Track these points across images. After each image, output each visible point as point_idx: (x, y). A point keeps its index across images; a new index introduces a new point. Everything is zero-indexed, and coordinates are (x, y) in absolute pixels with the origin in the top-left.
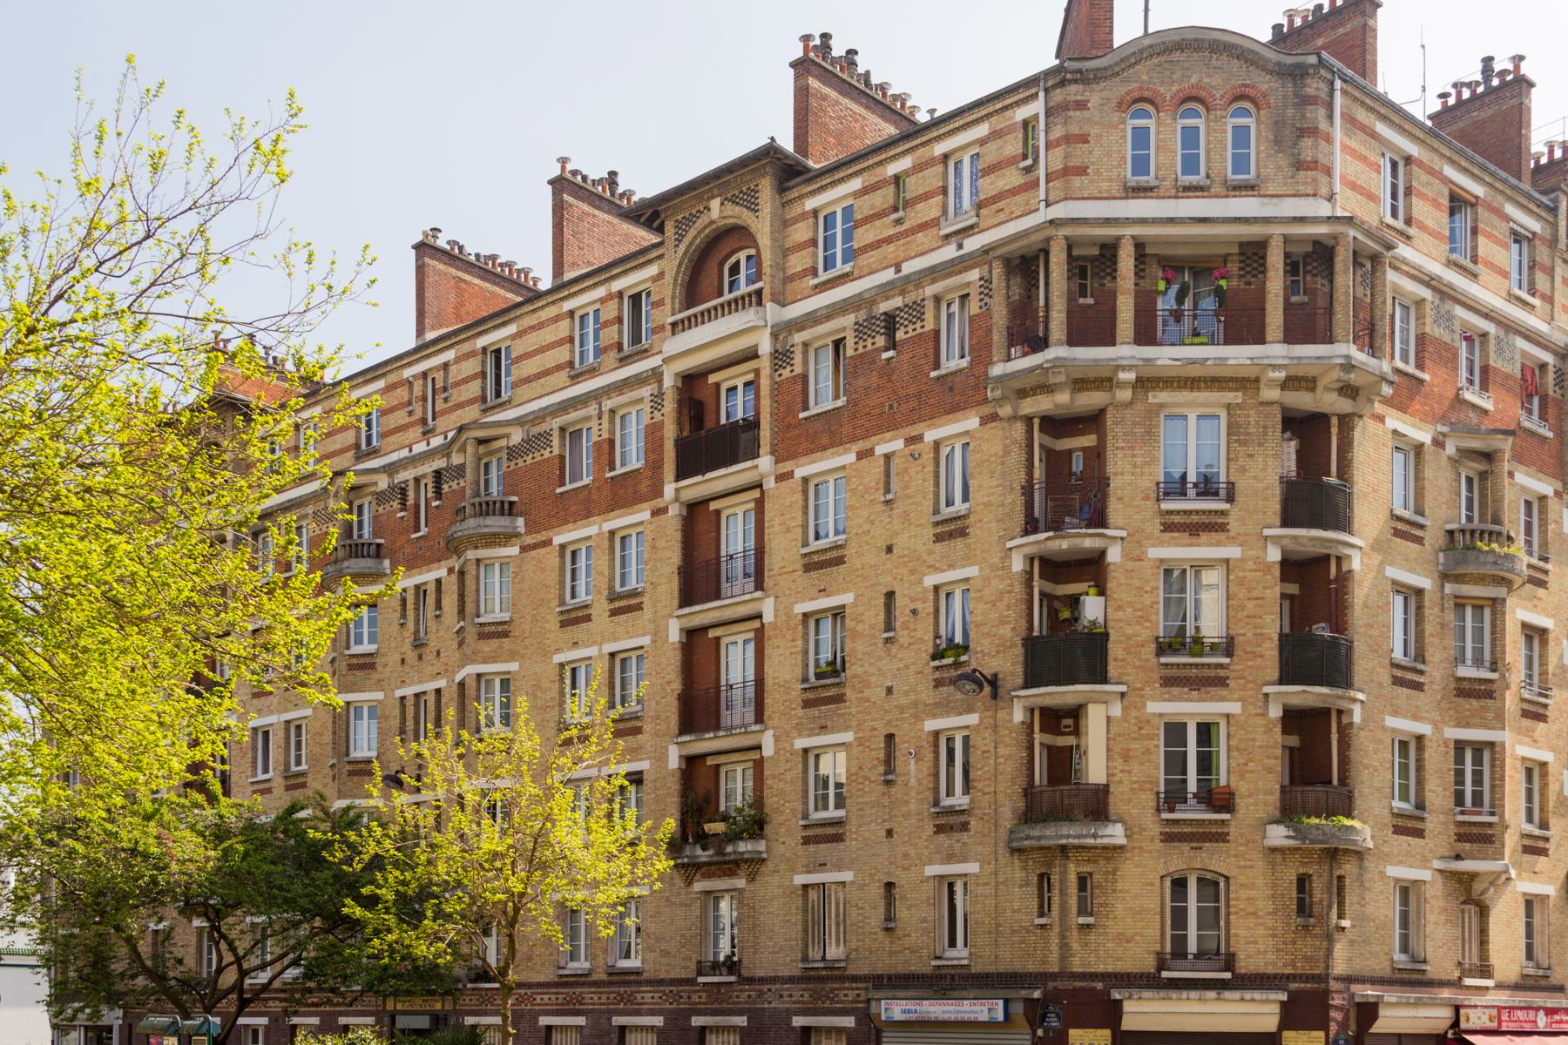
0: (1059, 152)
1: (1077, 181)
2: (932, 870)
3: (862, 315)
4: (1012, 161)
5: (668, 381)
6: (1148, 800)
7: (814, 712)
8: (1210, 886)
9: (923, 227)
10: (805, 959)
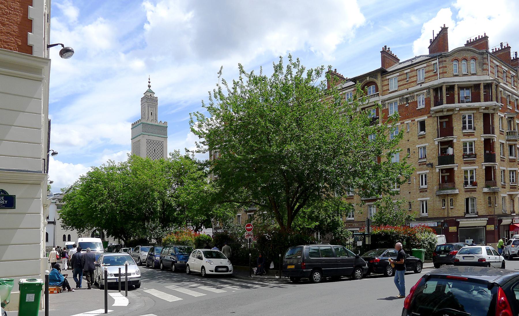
1: (445, 74)
2: (419, 199)
3: (401, 98)
4: (432, 71)
6: (462, 185)
8: (473, 199)
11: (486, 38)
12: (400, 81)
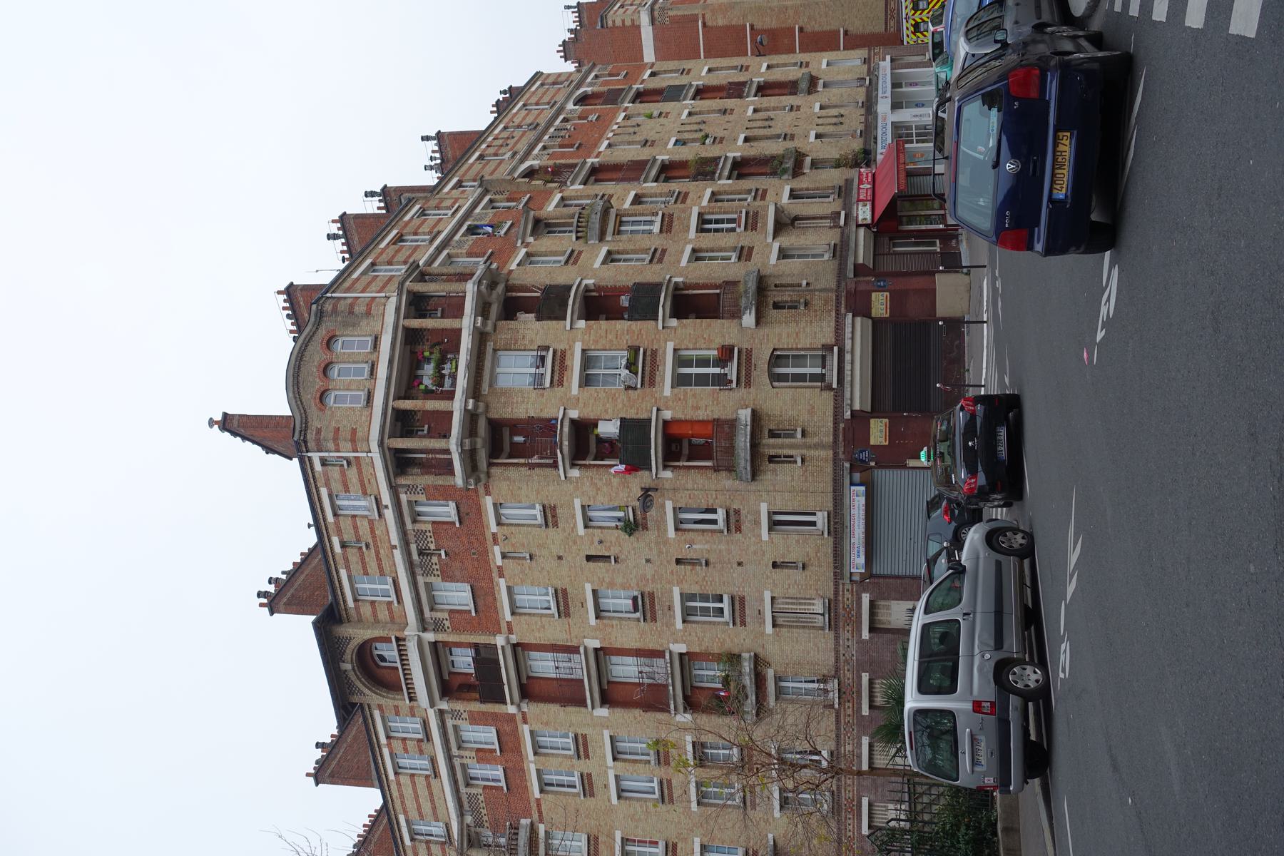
0: (342, 444)
1: (359, 434)
2: (765, 535)
4: (343, 473)
5: (444, 705)
6: (724, 395)
7: (659, 614)
9: (372, 530)
10: (822, 628)
11: (291, 292)
12: (364, 568)
